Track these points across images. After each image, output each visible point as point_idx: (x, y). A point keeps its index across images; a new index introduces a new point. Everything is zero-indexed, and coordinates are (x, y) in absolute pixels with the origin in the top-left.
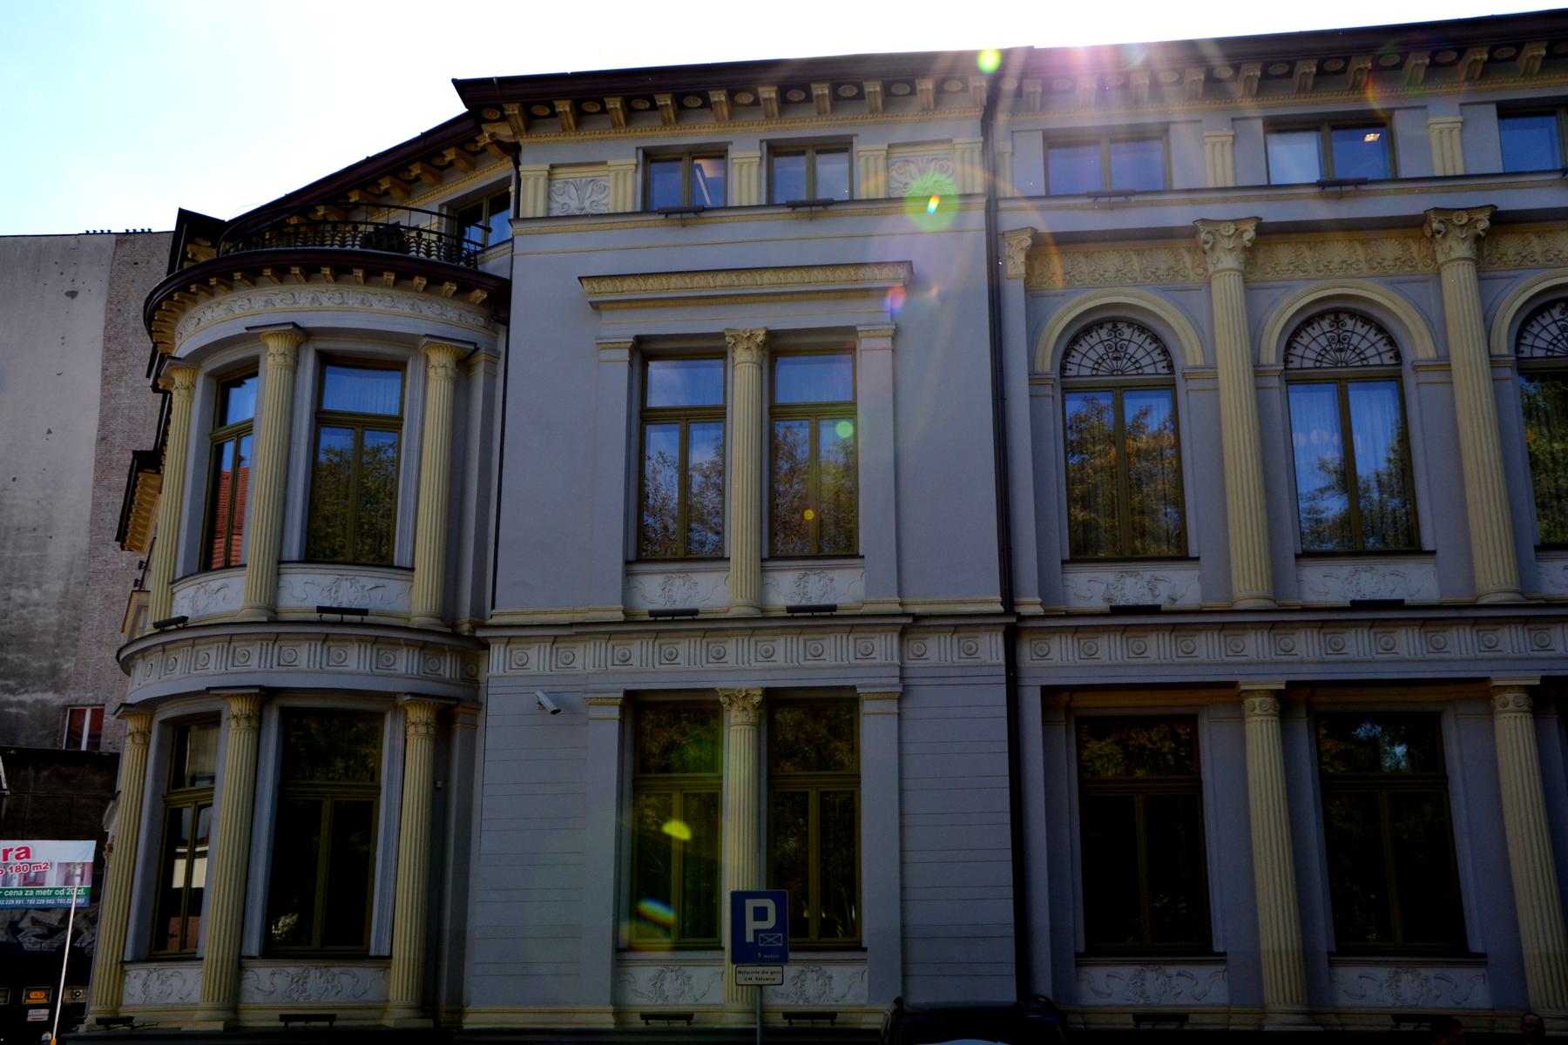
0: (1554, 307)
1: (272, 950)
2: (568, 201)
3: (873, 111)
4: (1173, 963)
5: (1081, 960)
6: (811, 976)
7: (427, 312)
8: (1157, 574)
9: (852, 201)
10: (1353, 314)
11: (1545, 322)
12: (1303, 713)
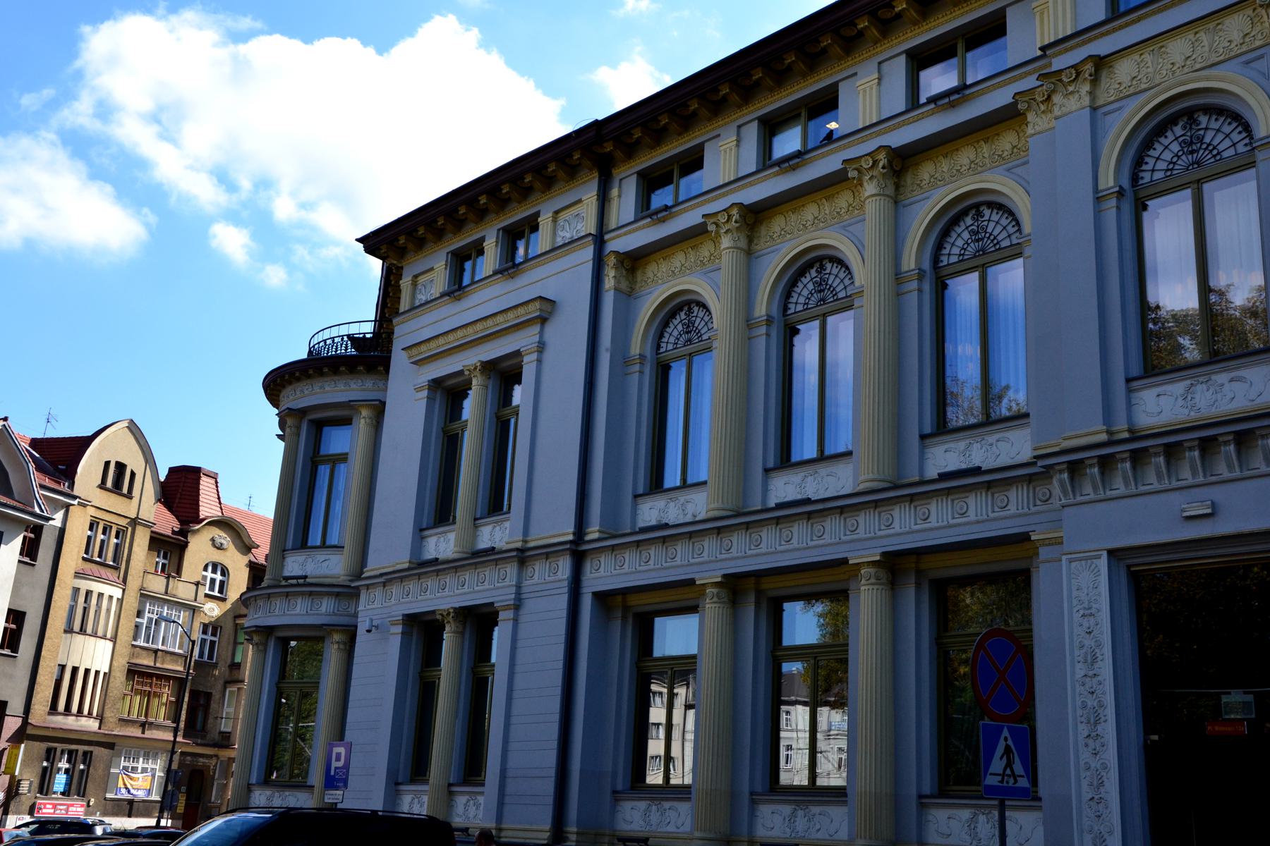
0: (967, 215)
1: (266, 782)
2: (421, 298)
3: (876, 42)
4: (667, 799)
5: (923, 802)
6: (800, 813)
7: (353, 386)
8: (688, 497)
9: (677, 204)
10: (990, 205)
11: (1149, 167)
12: (752, 598)
